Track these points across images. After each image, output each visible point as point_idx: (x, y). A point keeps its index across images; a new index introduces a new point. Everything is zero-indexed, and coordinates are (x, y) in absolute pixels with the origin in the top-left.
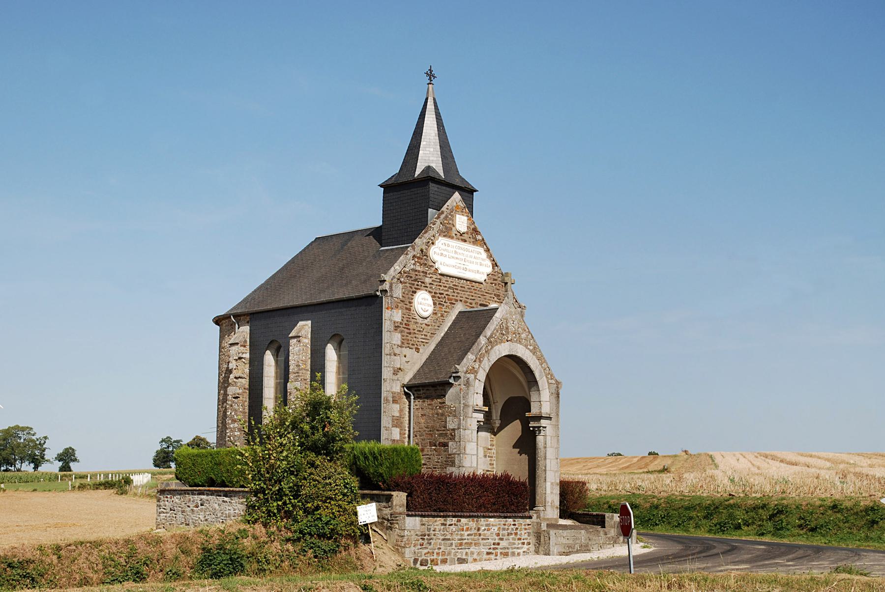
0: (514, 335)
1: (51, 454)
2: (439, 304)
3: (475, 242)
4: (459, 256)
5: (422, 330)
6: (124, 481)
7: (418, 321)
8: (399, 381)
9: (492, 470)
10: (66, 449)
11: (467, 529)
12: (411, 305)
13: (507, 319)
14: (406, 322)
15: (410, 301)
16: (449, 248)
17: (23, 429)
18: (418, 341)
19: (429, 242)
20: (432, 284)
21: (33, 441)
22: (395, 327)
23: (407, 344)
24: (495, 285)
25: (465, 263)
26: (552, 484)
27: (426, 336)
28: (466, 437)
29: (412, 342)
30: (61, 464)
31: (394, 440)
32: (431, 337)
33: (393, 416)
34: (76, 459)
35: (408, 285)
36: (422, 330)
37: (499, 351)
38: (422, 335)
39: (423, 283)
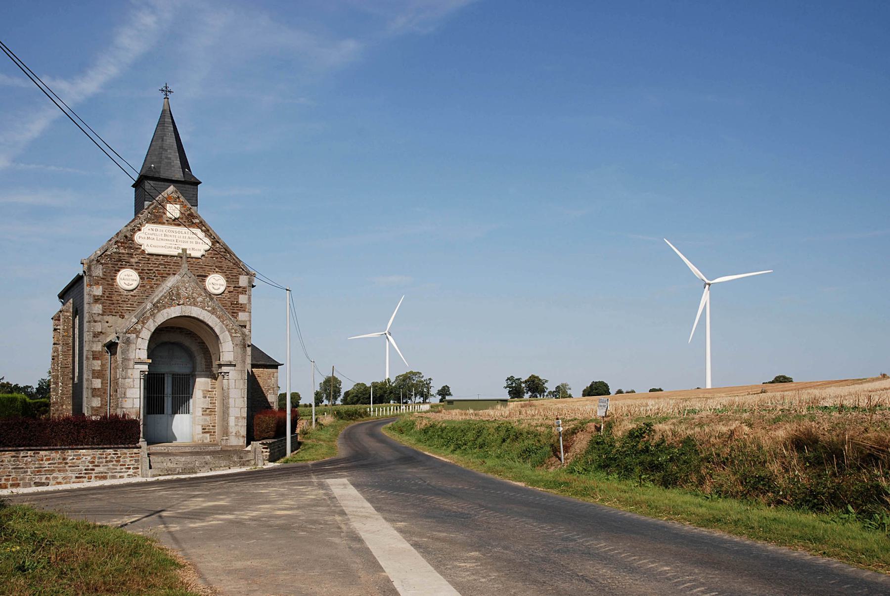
0: (188, 300)
1: (433, 391)
2: (147, 278)
3: (192, 225)
4: (169, 238)
6: (337, 413)
7: (122, 293)
8: (100, 342)
9: (214, 408)
10: (444, 387)
11: (49, 459)
13: (178, 288)
16: (158, 233)
19: (134, 229)
20: (139, 263)
21: (421, 382)
23: (110, 312)
24: (217, 258)
25: (176, 243)
26: (237, 418)
27: (133, 304)
28: (127, 384)
29: (116, 311)
30: (440, 397)
31: (95, 388)
34: (450, 394)
35: (110, 265)
36: (127, 300)
38: (127, 304)
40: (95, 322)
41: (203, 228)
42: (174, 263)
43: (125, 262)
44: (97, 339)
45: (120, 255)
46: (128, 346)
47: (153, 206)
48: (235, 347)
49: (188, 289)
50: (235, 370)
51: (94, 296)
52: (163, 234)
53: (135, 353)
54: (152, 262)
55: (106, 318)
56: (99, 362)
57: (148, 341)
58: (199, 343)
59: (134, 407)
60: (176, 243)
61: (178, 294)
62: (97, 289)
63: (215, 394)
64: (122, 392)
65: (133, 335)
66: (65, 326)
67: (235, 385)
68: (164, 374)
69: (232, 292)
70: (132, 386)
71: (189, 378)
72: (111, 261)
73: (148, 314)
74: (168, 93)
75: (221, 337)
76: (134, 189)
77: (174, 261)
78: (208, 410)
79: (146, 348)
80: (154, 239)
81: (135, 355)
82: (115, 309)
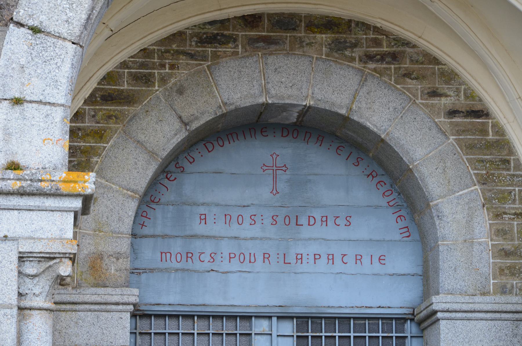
58: (452, 113)
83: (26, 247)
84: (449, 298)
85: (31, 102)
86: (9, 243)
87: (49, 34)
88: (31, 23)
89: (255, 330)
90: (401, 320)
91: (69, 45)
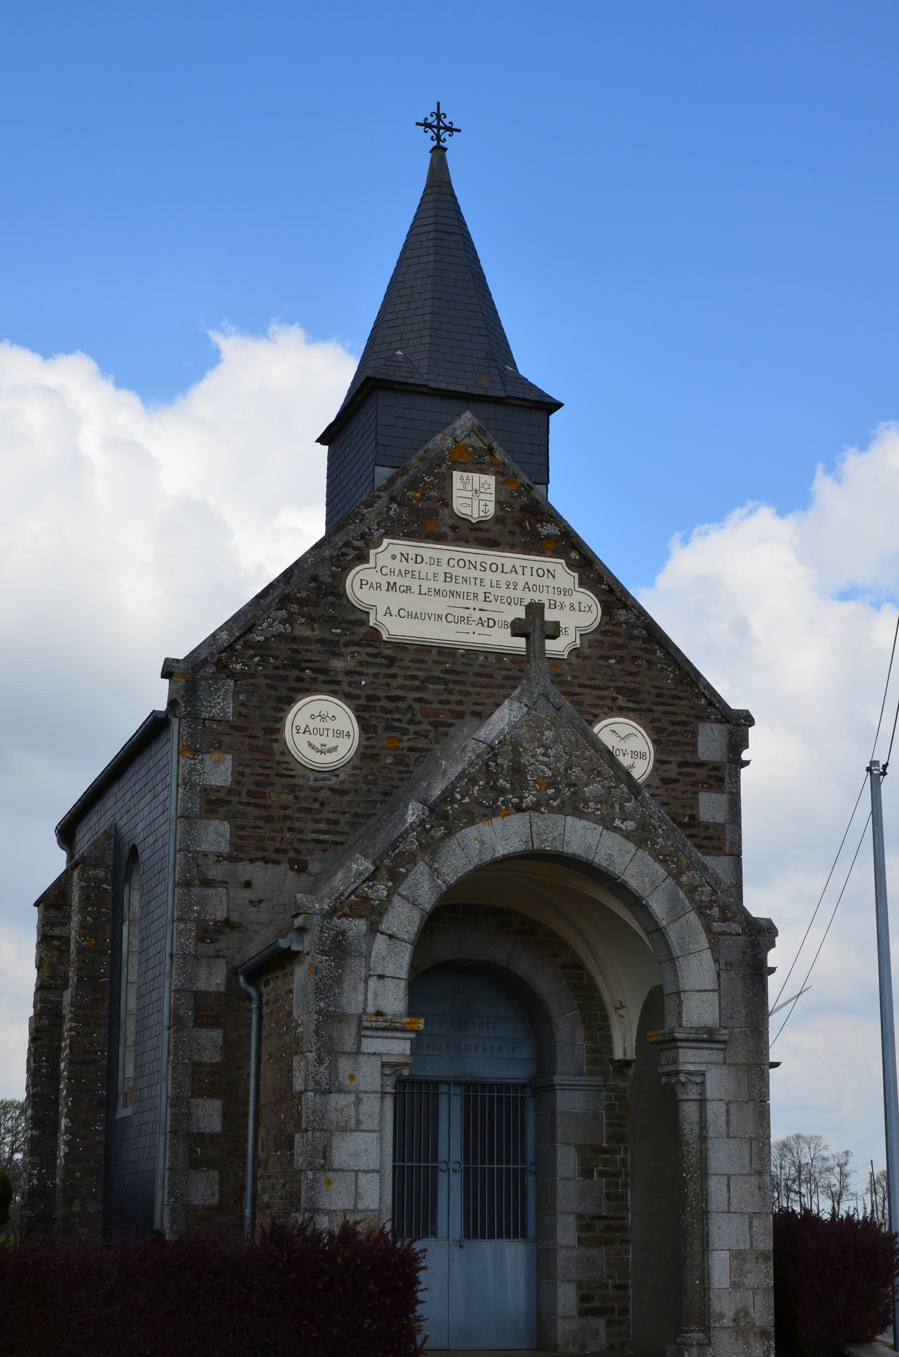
0: (551, 791)
2: (386, 729)
4: (462, 588)
5: (316, 805)
12: (274, 737)
14: (253, 788)
15: (271, 725)
16: (423, 568)
17: (808, 1141)
18: (302, 841)
22: (209, 802)
23: (257, 849)
24: (621, 660)
25: (485, 606)
26: (737, 1256)
27: (337, 822)
28: (333, 1116)
29: (278, 845)
31: (201, 1135)
32: (352, 825)
33: (198, 1064)
35: (261, 681)
37: (482, 842)
38: (318, 821)
39: (324, 672)
40: (207, 883)
41: (574, 555)
42: (475, 674)
43: (314, 670)
44: (211, 949)
45: (295, 646)
46: (337, 966)
47: (405, 478)
48: (723, 974)
49: (551, 752)
50: (725, 1063)
51: (206, 790)
52: (440, 571)
53: (366, 991)
54: (402, 672)
55: (246, 870)
56: (217, 1035)
57: (409, 948)
58: (564, 967)
59: (360, 1206)
60: (485, 606)
61: (518, 770)
62: (217, 763)
63: (624, 1162)
64: (314, 1148)
65: (357, 922)
66: (89, 914)
67: (728, 1123)
68: (436, 1084)
69: (676, 781)
70: (353, 1123)
71: (523, 1098)
72: (265, 667)
73: (412, 844)
74: (445, 135)
75: (673, 934)
76: (326, 448)
77: (477, 669)
78: (600, 1225)
79: (404, 974)
80: (409, 589)
81: (366, 999)
82: (273, 839)
83: (385, 1059)
84: (563, 1077)
85: (388, 977)
86: (377, 1057)
87: (398, 939)
88: (388, 932)
89: (441, 1090)
90: (523, 1087)
91: (408, 945)
